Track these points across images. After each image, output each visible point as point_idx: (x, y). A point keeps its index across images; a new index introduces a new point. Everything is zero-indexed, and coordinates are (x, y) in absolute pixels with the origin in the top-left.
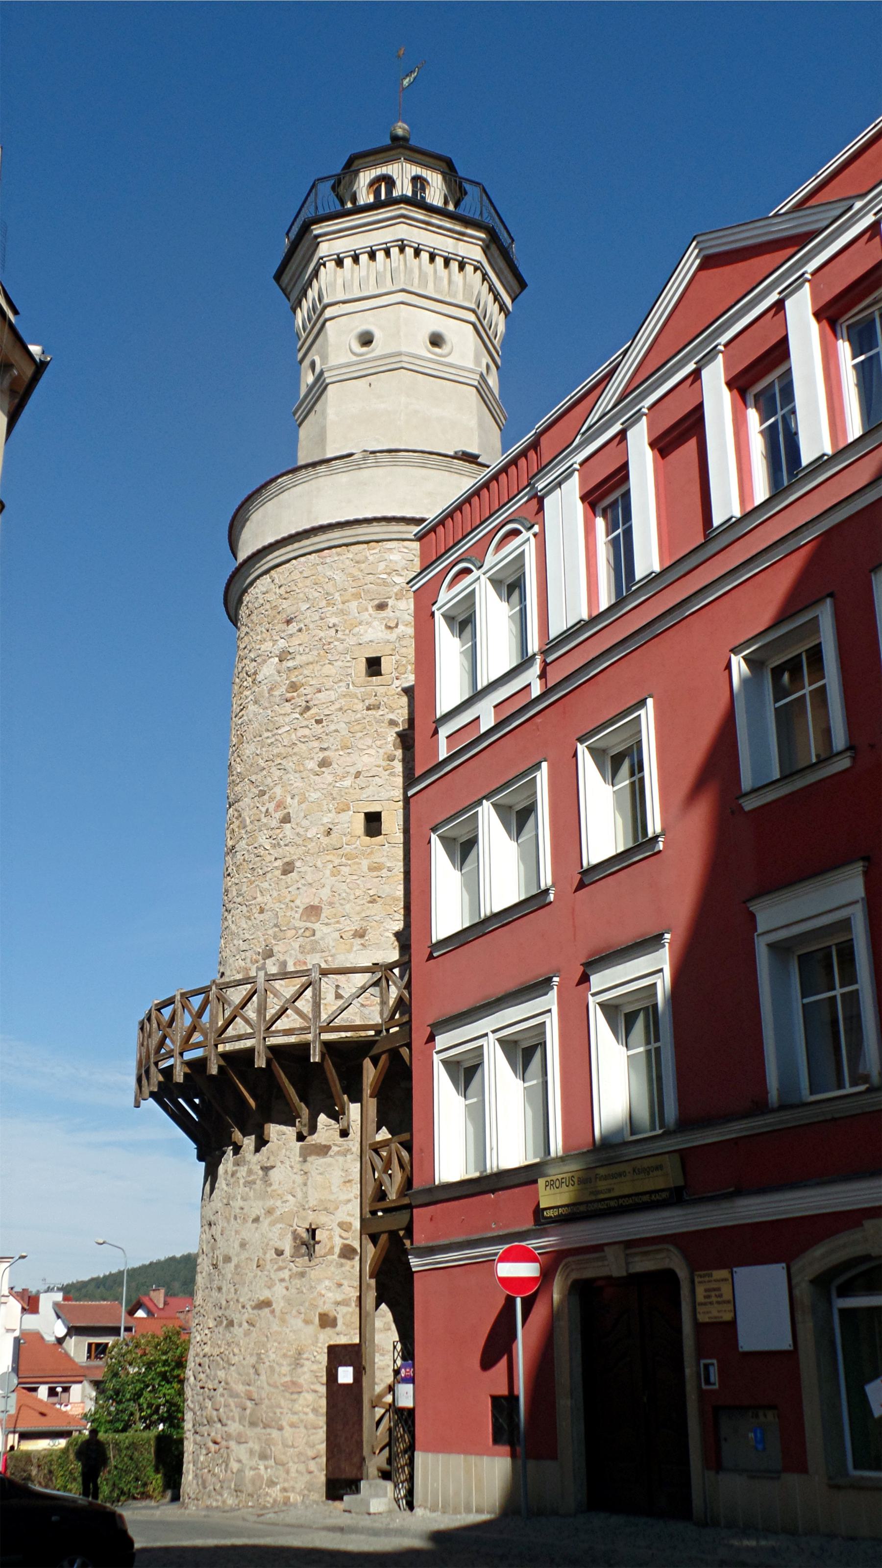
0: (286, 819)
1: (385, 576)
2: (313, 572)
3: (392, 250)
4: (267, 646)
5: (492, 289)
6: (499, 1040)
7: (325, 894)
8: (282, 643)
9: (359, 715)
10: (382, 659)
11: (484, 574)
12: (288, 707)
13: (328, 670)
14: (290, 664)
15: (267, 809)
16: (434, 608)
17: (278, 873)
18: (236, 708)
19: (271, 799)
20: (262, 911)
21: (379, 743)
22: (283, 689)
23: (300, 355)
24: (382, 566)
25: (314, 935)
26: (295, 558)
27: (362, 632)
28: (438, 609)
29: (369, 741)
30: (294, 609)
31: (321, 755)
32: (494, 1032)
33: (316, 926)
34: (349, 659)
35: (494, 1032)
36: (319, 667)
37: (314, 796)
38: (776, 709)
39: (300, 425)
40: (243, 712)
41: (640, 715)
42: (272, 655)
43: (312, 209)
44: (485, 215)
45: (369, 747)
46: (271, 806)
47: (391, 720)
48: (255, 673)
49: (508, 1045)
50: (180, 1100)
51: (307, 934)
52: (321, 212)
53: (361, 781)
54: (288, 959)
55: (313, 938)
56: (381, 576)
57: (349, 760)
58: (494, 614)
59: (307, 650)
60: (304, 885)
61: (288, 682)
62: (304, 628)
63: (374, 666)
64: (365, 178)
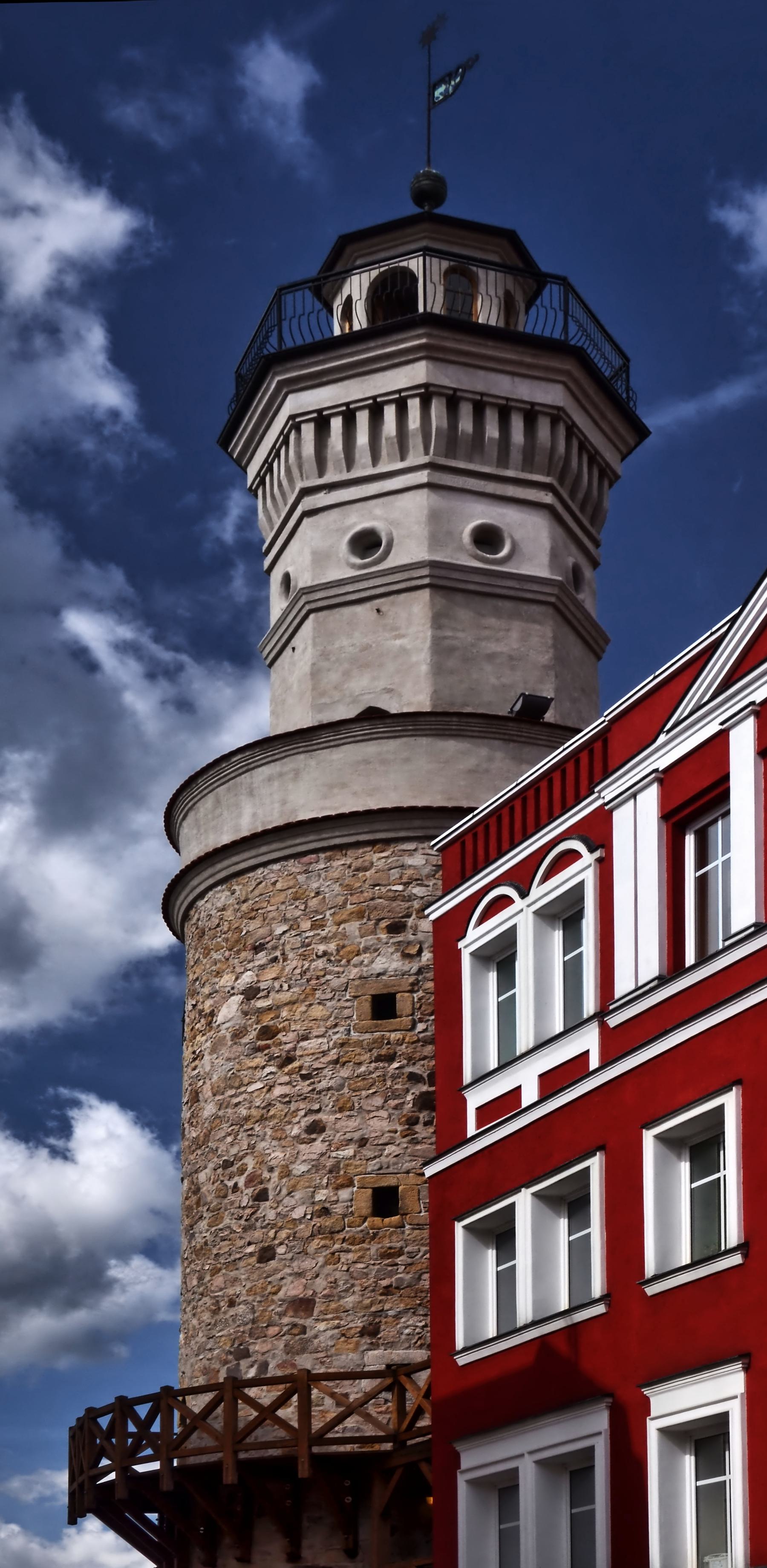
0: (262, 1196)
1: (400, 888)
2: (291, 883)
3: (410, 402)
4: (227, 980)
5: (584, 446)
6: (538, 1463)
7: (321, 1284)
8: (247, 978)
9: (363, 1069)
10: (398, 996)
11: (529, 906)
12: (260, 1060)
13: (317, 1011)
14: (261, 1004)
15: (236, 1184)
16: (461, 944)
17: (253, 1260)
18: (187, 1054)
19: (242, 1171)
20: (232, 1304)
21: (393, 1103)
22: (253, 1034)
23: (267, 562)
24: (395, 874)
25: (305, 1333)
26: (265, 864)
27: (366, 962)
28: (465, 947)
29: (378, 1101)
30: (261, 931)
31: (310, 1119)
32: (531, 1453)
33: (309, 1322)
34: (348, 997)
35: (531, 1453)
36: (303, 1008)
37: (300, 1168)
38: (498, 1273)
39: (271, 665)
40: (197, 1062)
41: (588, 1168)
42: (236, 991)
43: (272, 343)
44: (573, 328)
45: (378, 1109)
46: (241, 1181)
47: (411, 1073)
48: (212, 1014)
49: (550, 1466)
50: (430, 1436)
51: (295, 1331)
52: (289, 344)
53: (368, 1152)
54: (269, 1360)
55: (302, 1336)
56: (394, 888)
57: (353, 1124)
58: (539, 957)
59: (286, 987)
60: (290, 1275)
61: (259, 1027)
62: (280, 957)
63: (383, 1006)
64: (357, 287)
